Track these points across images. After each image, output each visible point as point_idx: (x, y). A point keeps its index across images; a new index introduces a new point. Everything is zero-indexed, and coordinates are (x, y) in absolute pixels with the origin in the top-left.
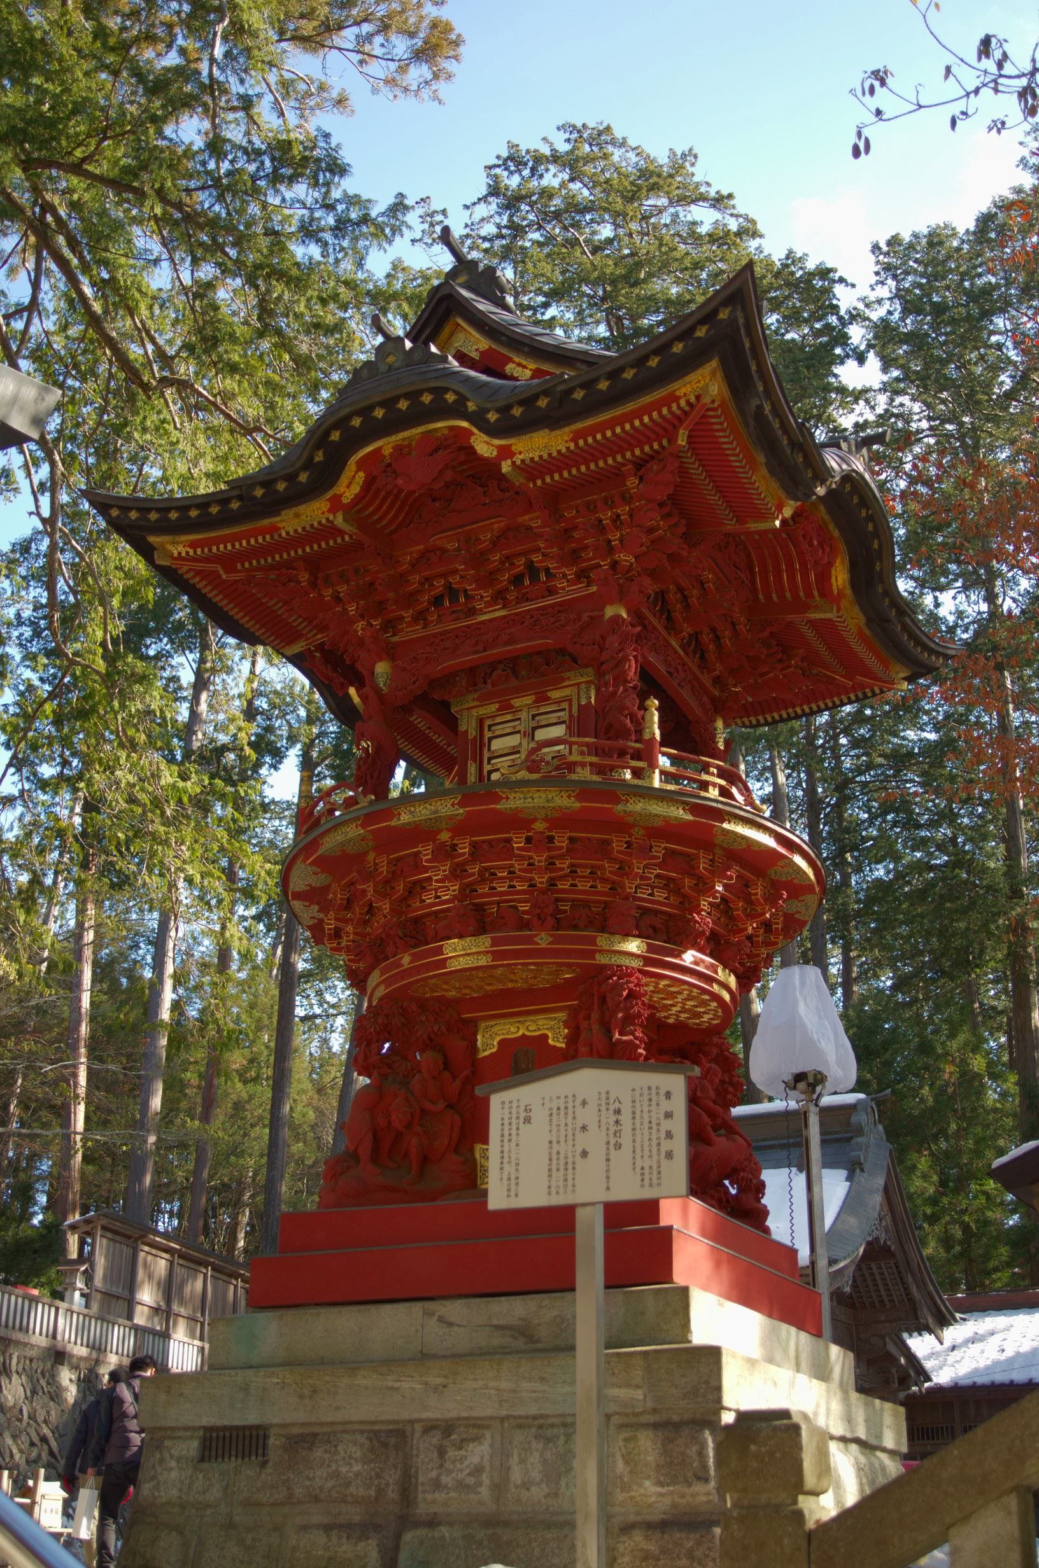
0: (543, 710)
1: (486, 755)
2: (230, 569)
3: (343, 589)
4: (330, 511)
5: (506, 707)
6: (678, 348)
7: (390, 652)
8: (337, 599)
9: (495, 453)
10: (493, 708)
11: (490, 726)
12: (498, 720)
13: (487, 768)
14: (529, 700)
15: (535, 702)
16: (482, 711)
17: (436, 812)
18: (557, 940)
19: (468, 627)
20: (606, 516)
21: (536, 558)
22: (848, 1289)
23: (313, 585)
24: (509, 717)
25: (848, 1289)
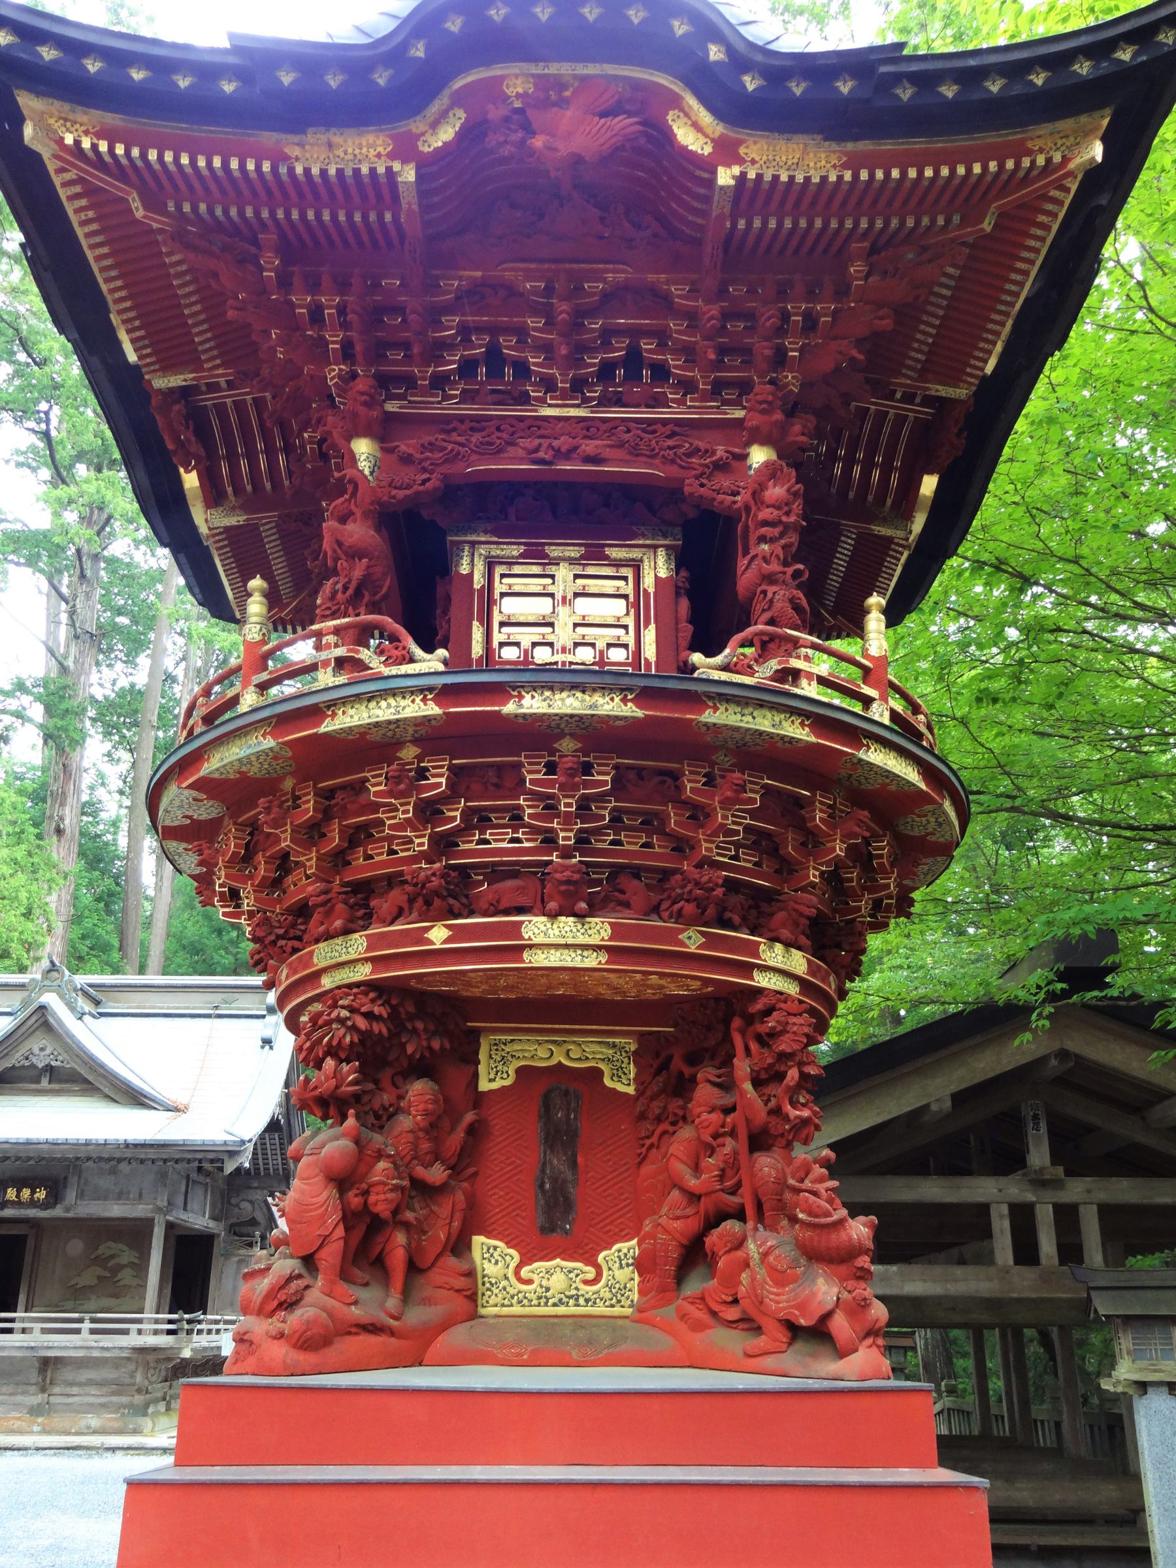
0: (591, 571)
1: (497, 618)
2: (153, 203)
3: (330, 302)
4: (392, 156)
5: (535, 554)
6: (1083, 68)
7: (385, 431)
8: (316, 313)
9: (708, 150)
10: (515, 551)
11: (503, 576)
12: (517, 570)
13: (497, 638)
14: (574, 552)
15: (582, 557)
16: (496, 551)
17: (594, 706)
18: (712, 941)
19: (521, 419)
20: (796, 310)
21: (647, 345)
22: (247, 1165)
23: (284, 282)
24: (536, 570)
25: (247, 1165)
